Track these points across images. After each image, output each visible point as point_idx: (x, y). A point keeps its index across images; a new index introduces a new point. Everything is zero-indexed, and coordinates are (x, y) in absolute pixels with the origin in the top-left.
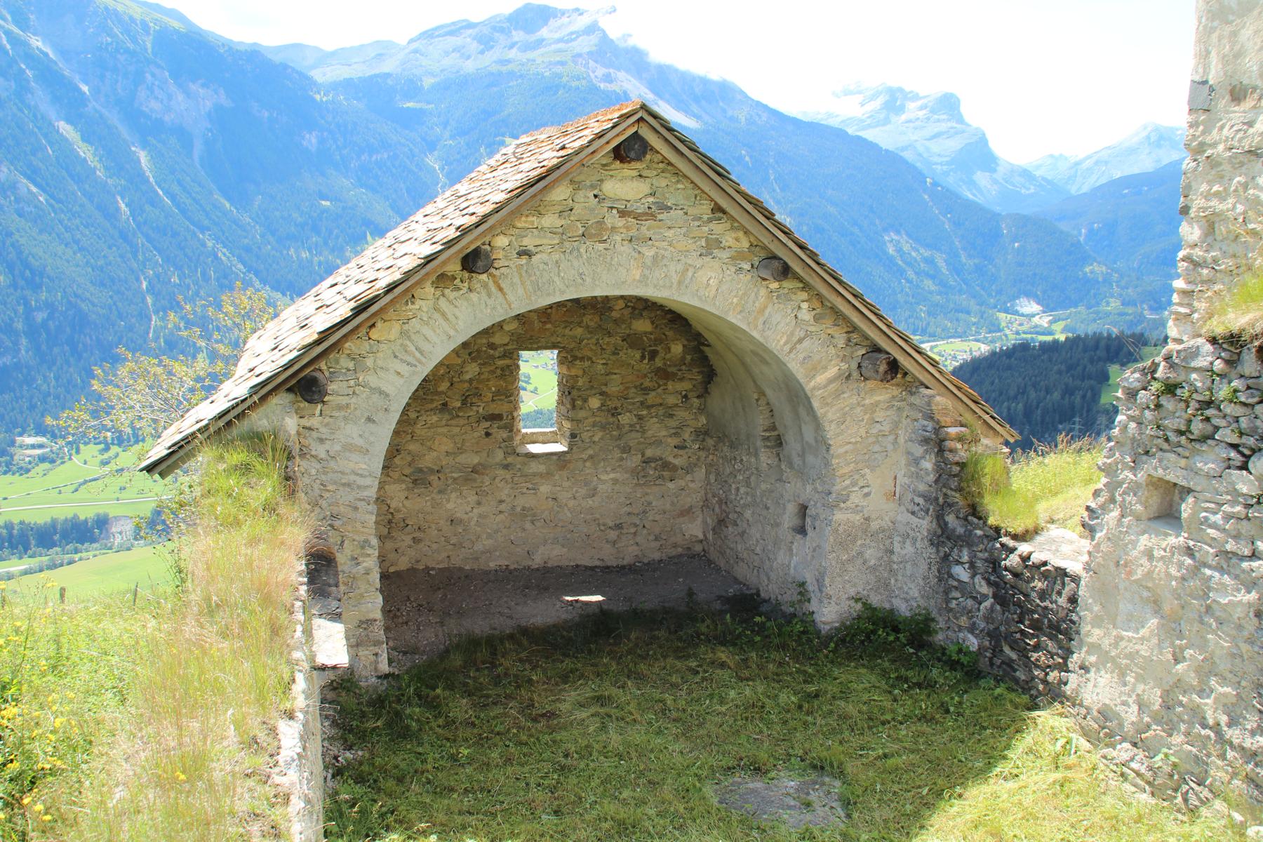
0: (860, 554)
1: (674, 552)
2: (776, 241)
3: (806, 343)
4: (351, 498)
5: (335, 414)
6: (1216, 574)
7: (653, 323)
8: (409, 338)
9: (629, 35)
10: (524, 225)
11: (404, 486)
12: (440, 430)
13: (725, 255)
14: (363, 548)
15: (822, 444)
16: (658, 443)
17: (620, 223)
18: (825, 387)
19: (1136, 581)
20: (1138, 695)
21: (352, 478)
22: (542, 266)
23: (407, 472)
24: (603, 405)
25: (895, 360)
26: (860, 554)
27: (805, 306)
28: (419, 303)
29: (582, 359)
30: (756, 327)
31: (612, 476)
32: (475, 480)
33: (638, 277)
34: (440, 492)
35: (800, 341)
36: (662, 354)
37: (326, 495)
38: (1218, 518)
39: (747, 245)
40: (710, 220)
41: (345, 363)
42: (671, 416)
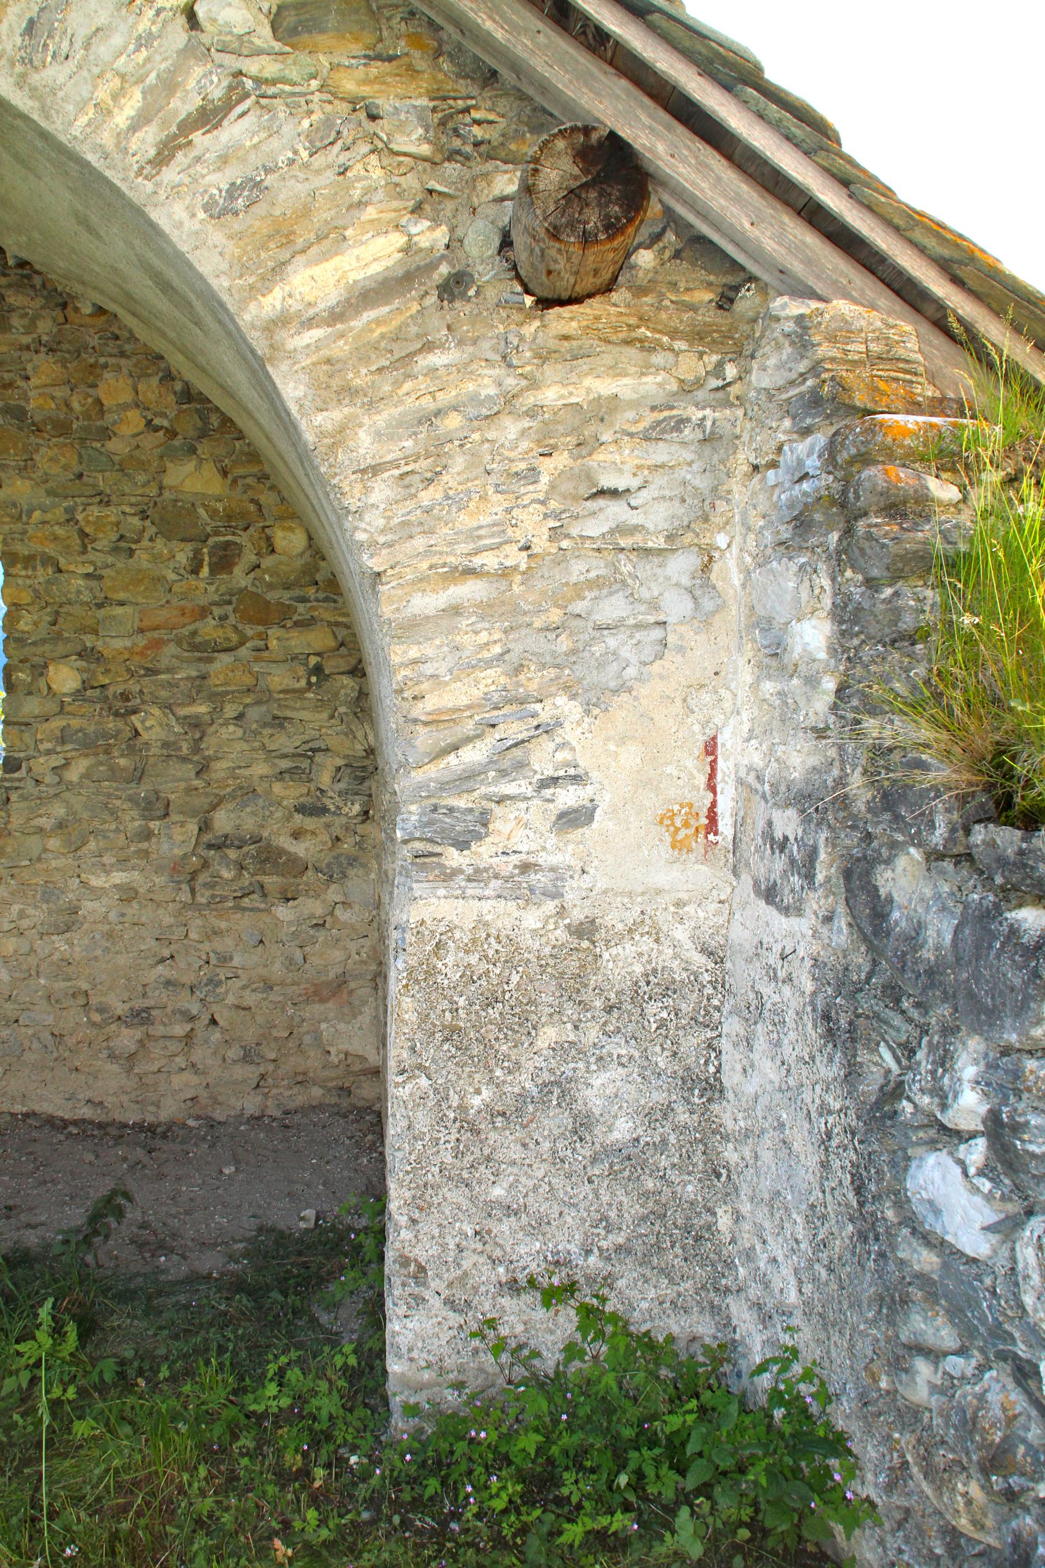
0: (558, 1089)
1: (299, 1098)
3: (235, 130)
7: (224, 473)
16: (247, 793)
18: (336, 316)
24: (86, 685)
26: (558, 1089)
31: (118, 877)
35: (209, 117)
36: (249, 557)
42: (279, 722)
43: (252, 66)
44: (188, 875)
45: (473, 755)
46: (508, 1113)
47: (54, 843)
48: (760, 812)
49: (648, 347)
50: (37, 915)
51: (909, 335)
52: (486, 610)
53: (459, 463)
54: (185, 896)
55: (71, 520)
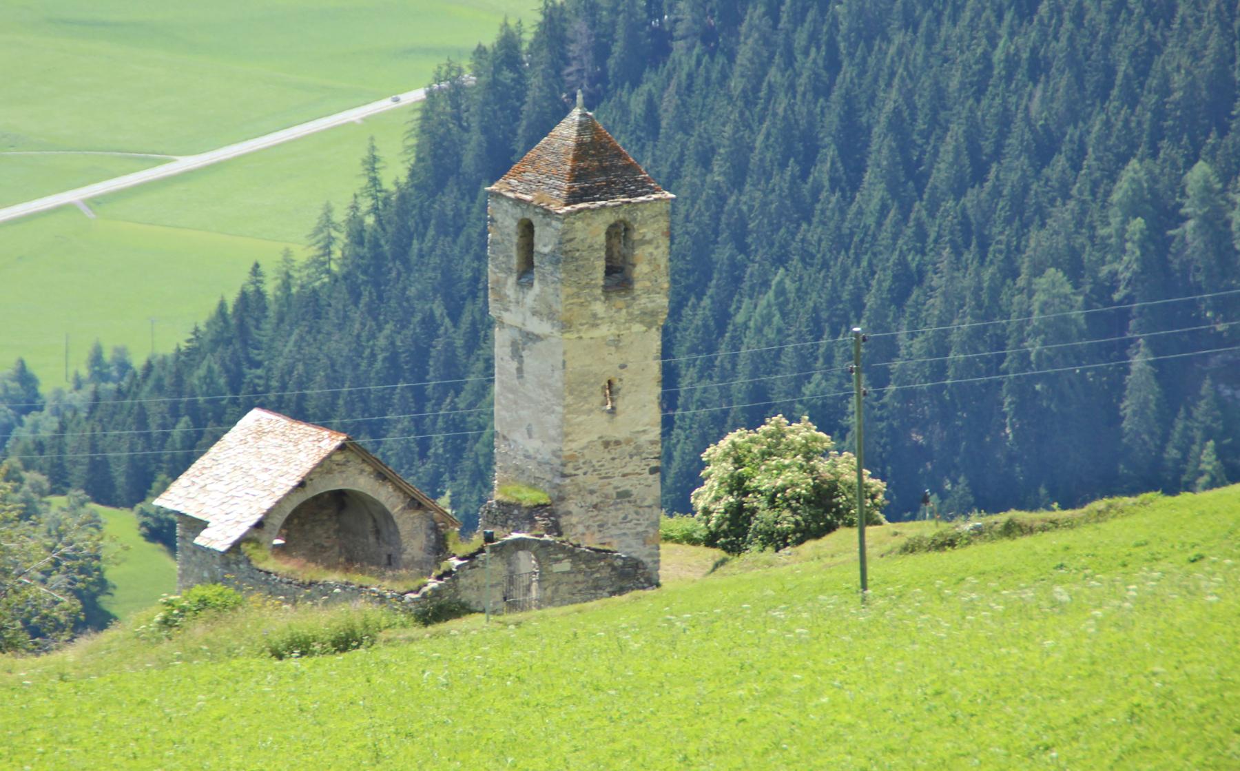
9: (203, 525)
15: (396, 532)
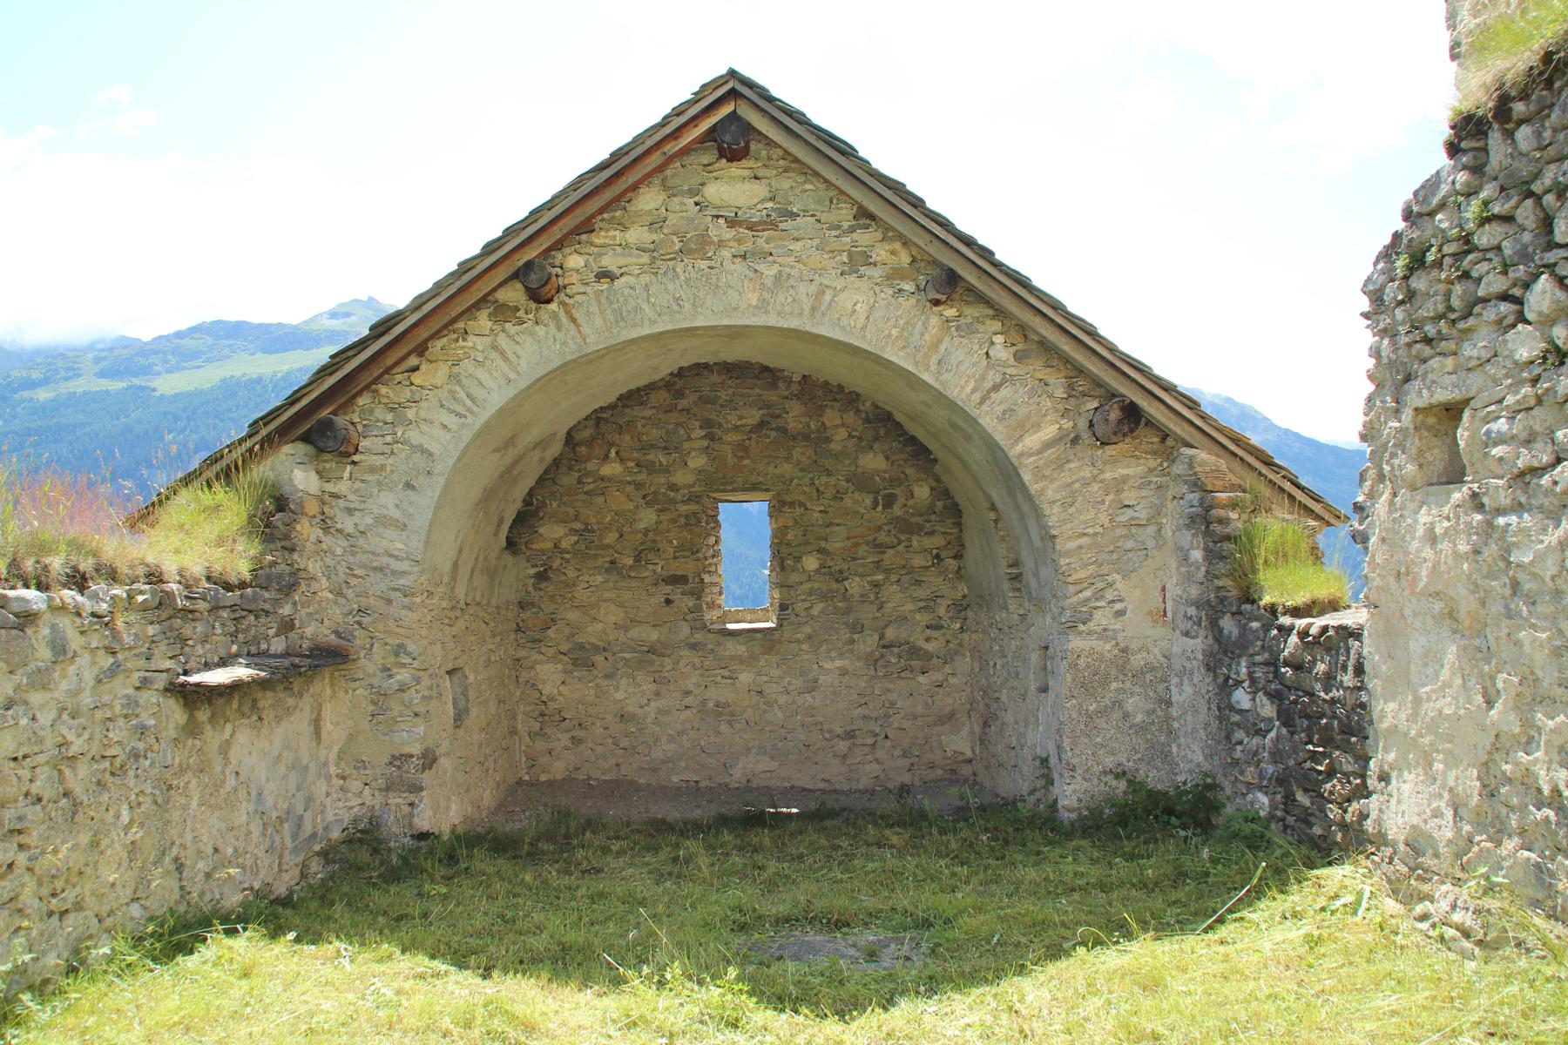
0: (1117, 704)
2: (936, 242)
3: (1005, 392)
4: (383, 587)
5: (367, 477)
6: (1513, 519)
7: (887, 458)
8: (459, 382)
10: (603, 241)
11: (560, 667)
12: (607, 595)
13: (876, 273)
14: (397, 655)
17: (729, 234)
18: (1039, 452)
19: (1422, 594)
20: (1451, 790)
21: (386, 560)
22: (627, 291)
23: (564, 648)
24: (822, 566)
25: (1132, 404)
26: (1117, 704)
27: (999, 339)
28: (472, 340)
29: (792, 504)
30: (927, 368)
31: (839, 663)
32: (652, 663)
33: (754, 302)
34: (606, 676)
35: (996, 388)
36: (901, 500)
37: (354, 582)
38: (1501, 425)
39: (909, 260)
40: (852, 230)
41: (381, 413)
42: (918, 583)
43: (1009, 371)
44: (873, 661)
45: (1087, 594)
46: (1103, 712)
47: (804, 647)
48: (1182, 609)
49: (1138, 458)
50: (798, 683)
51: (1223, 464)
52: (1090, 547)
53: (1080, 499)
54: (872, 672)
55: (812, 484)
